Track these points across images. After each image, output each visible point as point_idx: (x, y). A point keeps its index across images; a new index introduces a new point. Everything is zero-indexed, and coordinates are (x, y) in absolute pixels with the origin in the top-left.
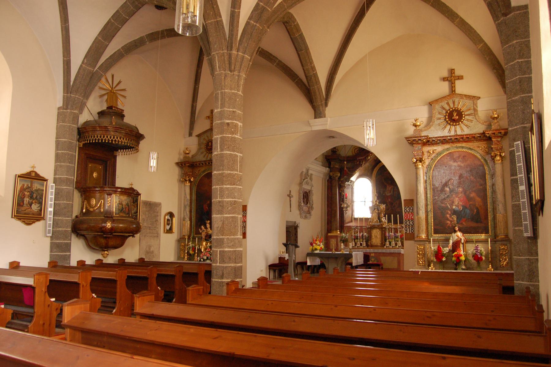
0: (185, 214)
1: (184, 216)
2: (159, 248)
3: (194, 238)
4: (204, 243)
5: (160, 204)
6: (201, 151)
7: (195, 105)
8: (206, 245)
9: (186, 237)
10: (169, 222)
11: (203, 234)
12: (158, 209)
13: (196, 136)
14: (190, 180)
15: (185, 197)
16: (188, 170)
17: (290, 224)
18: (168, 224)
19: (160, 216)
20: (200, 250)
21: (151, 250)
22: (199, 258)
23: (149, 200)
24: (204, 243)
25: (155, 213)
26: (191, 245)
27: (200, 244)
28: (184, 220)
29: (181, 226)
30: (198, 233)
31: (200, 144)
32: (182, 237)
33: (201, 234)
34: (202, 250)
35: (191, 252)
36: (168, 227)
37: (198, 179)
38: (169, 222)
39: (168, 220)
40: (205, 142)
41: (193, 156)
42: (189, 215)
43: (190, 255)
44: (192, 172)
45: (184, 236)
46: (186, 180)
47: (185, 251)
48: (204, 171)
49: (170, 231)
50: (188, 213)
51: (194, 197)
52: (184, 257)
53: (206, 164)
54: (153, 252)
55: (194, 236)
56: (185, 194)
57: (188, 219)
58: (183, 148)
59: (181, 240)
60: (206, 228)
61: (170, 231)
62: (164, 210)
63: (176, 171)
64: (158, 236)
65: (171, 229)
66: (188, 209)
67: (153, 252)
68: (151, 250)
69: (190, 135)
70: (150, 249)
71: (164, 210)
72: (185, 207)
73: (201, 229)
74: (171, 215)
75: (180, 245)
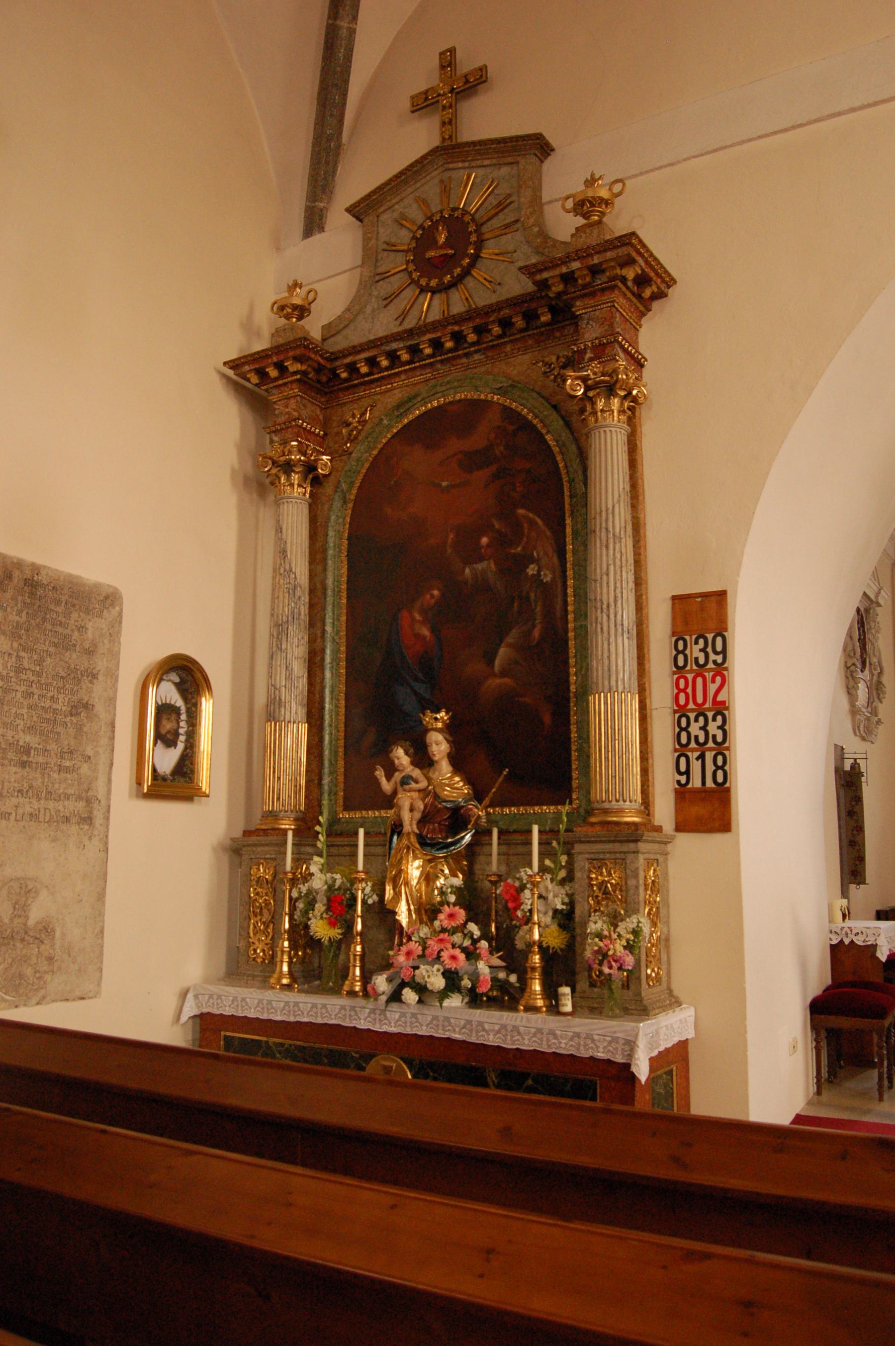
0: (281, 679)
1: (273, 687)
2: (101, 896)
3: (340, 835)
4: (414, 869)
5: (108, 600)
6: (385, 288)
7: (344, 24)
8: (428, 878)
9: (287, 825)
10: (174, 726)
11: (405, 800)
12: (94, 627)
13: (349, 210)
14: (310, 468)
15: (282, 570)
16: (291, 403)
17: (134, 793)
18: (166, 739)
19: (113, 675)
20: (382, 913)
21: (35, 915)
22: (381, 982)
23: (29, 555)
24: (414, 869)
25: (73, 658)
26: (319, 882)
27: (386, 874)
28: (271, 716)
29: (251, 754)
30: (364, 794)
31: (370, 255)
32: (256, 822)
33: (389, 801)
34: (403, 917)
35: (320, 928)
36: (166, 760)
37: (363, 455)
38: (174, 726)
39: (164, 710)
40: (404, 237)
41: (330, 331)
42: (302, 683)
43: (314, 943)
44: (325, 424)
45: (272, 815)
46: (288, 467)
47: (275, 920)
48: (402, 406)
49: (178, 784)
50: (299, 669)
51: (337, 572)
52: (272, 961)
53: (414, 350)
54: (46, 930)
55: (334, 821)
56: (283, 553)
57: (295, 709)
58: (268, 292)
59: (249, 845)
60: (423, 759)
61: (178, 784)
62: (139, 648)
63: (223, 427)
64: (89, 815)
65: (186, 768)
66: (296, 649)
67: (46, 930)
68: (35, 915)
69: (313, 223)
70: (20, 909)
71: (139, 648)
72: (279, 630)
73: (391, 769)
74: (187, 675)
75: (247, 879)
